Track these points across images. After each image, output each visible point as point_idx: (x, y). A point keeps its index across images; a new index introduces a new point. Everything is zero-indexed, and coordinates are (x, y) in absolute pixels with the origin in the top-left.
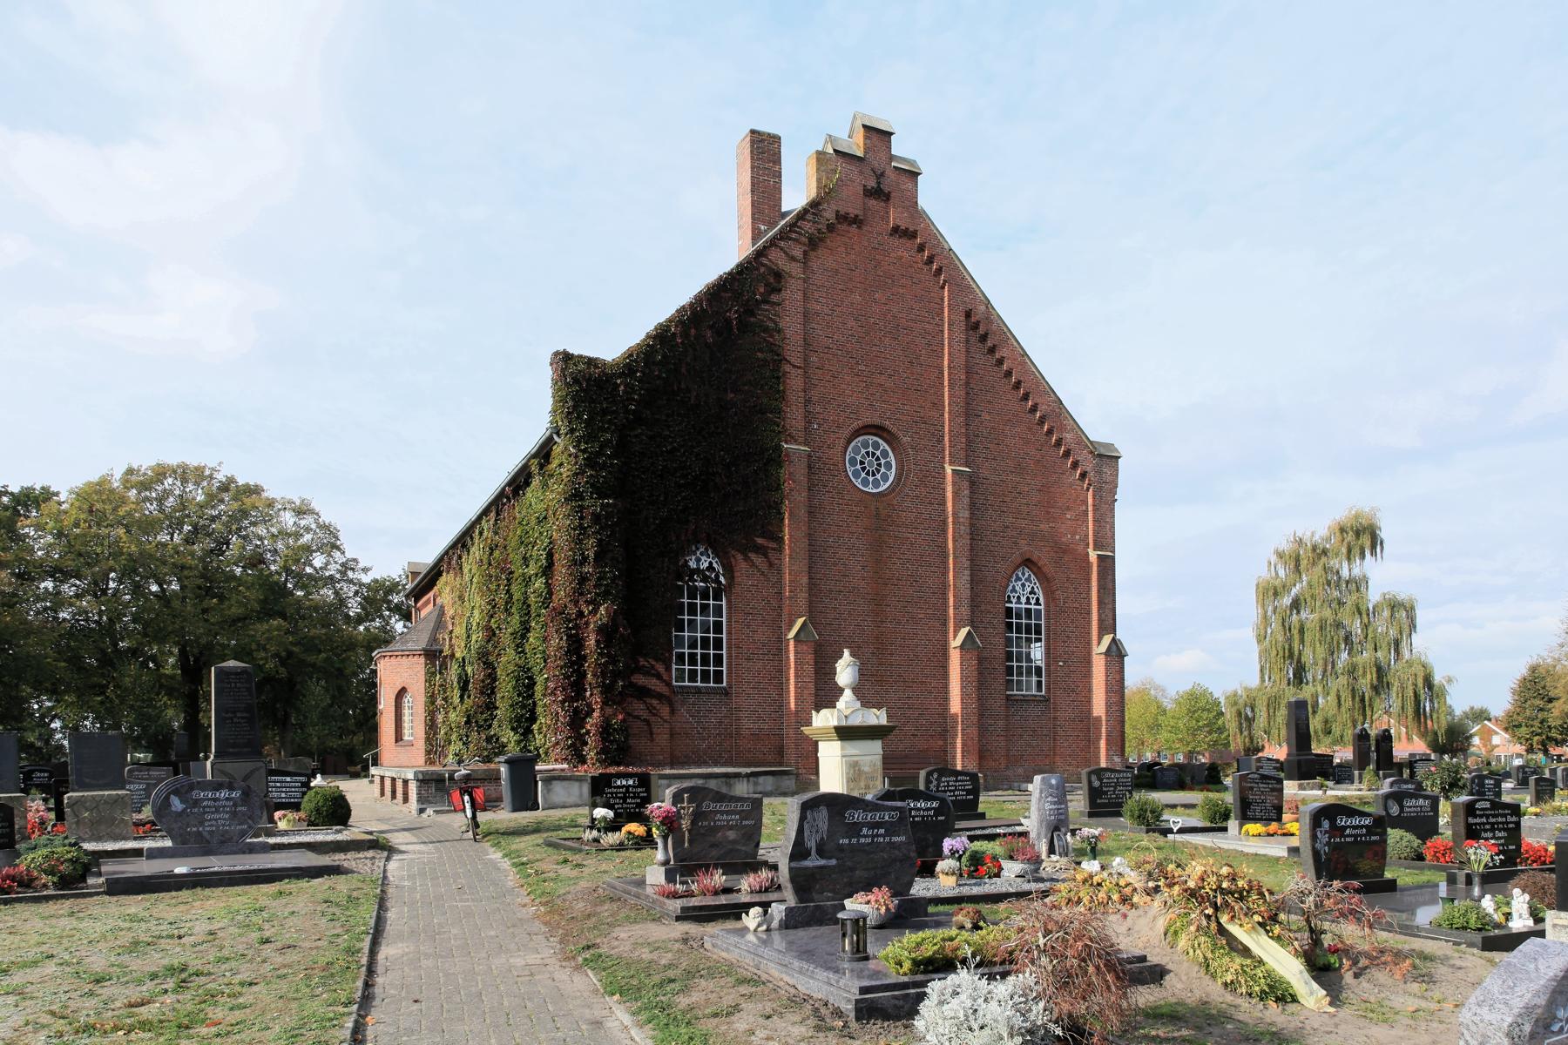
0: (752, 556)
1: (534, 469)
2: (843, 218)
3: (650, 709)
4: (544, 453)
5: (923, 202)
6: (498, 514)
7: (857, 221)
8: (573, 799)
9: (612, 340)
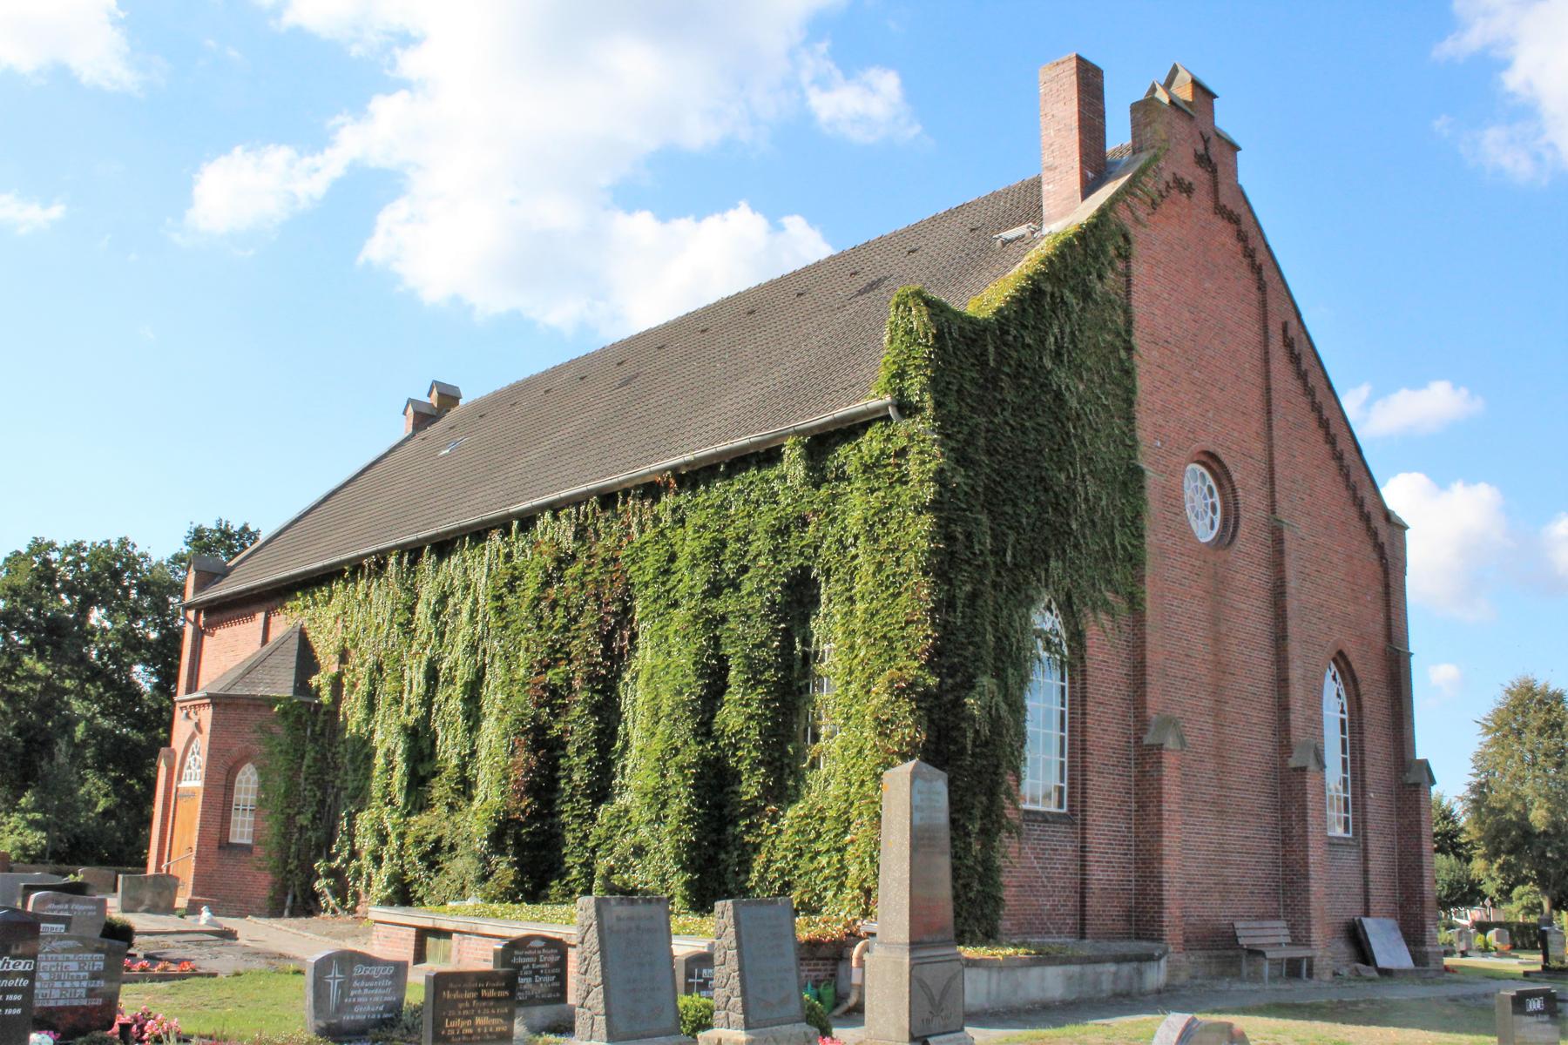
7: (1188, 190)
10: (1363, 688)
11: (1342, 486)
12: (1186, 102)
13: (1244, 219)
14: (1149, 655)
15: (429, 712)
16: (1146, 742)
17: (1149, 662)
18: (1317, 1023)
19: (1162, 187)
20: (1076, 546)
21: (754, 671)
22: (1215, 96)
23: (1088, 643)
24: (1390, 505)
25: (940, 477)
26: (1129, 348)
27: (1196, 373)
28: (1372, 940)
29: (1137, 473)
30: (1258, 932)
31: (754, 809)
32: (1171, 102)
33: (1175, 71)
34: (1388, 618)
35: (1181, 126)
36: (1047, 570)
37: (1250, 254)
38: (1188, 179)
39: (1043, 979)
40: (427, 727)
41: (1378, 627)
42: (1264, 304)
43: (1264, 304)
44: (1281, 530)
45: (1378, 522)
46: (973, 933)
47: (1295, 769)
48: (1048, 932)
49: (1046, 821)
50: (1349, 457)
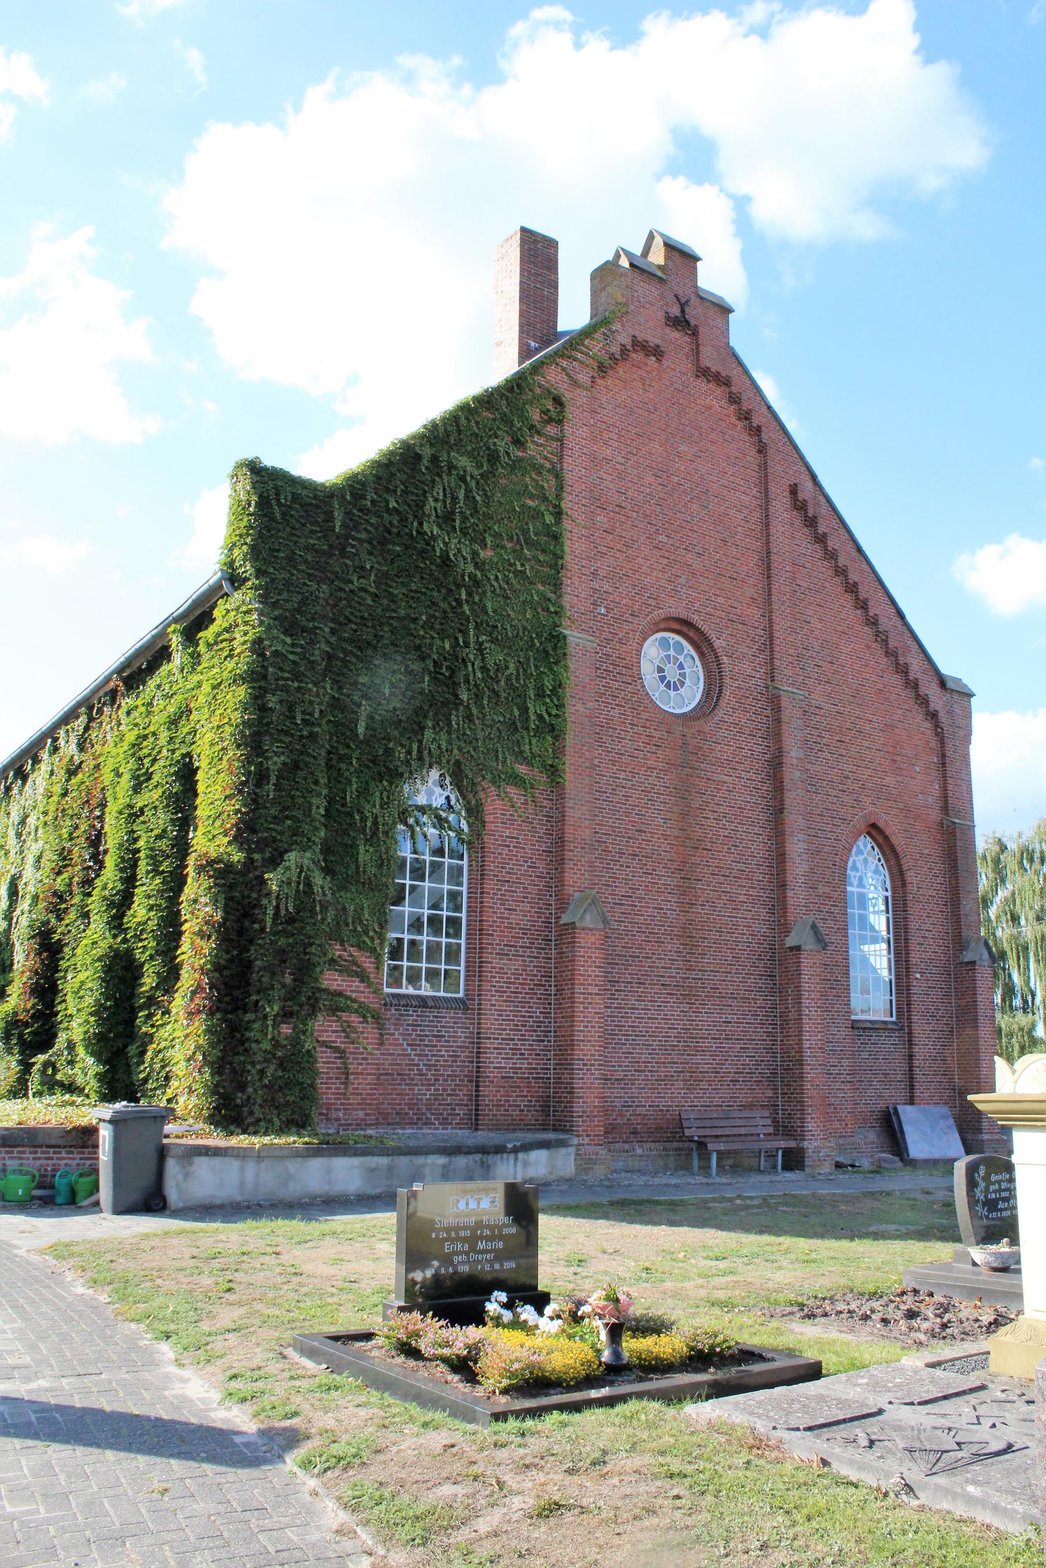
0: (512, 790)
1: (175, 641)
2: (639, 345)
3: (347, 1030)
4: (196, 619)
5: (732, 343)
6: (91, 719)
7: (657, 352)
8: (202, 1166)
9: (329, 457)
10: (907, 863)
11: (880, 652)
12: (659, 267)
13: (735, 380)
14: (569, 830)
15: (10, 925)
16: (562, 922)
17: (568, 837)
18: (638, 1227)
19: (615, 349)
20: (469, 717)
21: (155, 861)
22: (697, 259)
23: (489, 818)
24: (945, 669)
25: (257, 646)
26: (559, 514)
27: (663, 538)
28: (907, 1129)
29: (557, 640)
30: (722, 1123)
31: (151, 1001)
32: (632, 265)
33: (651, 237)
34: (944, 789)
35: (646, 291)
36: (420, 742)
37: (746, 416)
38: (654, 341)
39: (329, 1171)
40: (8, 939)
41: (932, 799)
42: (764, 466)
43: (764, 466)
44: (778, 697)
45: (931, 690)
46: (270, 1121)
47: (791, 949)
48: (428, 1123)
49: (425, 1006)
50: (887, 622)
